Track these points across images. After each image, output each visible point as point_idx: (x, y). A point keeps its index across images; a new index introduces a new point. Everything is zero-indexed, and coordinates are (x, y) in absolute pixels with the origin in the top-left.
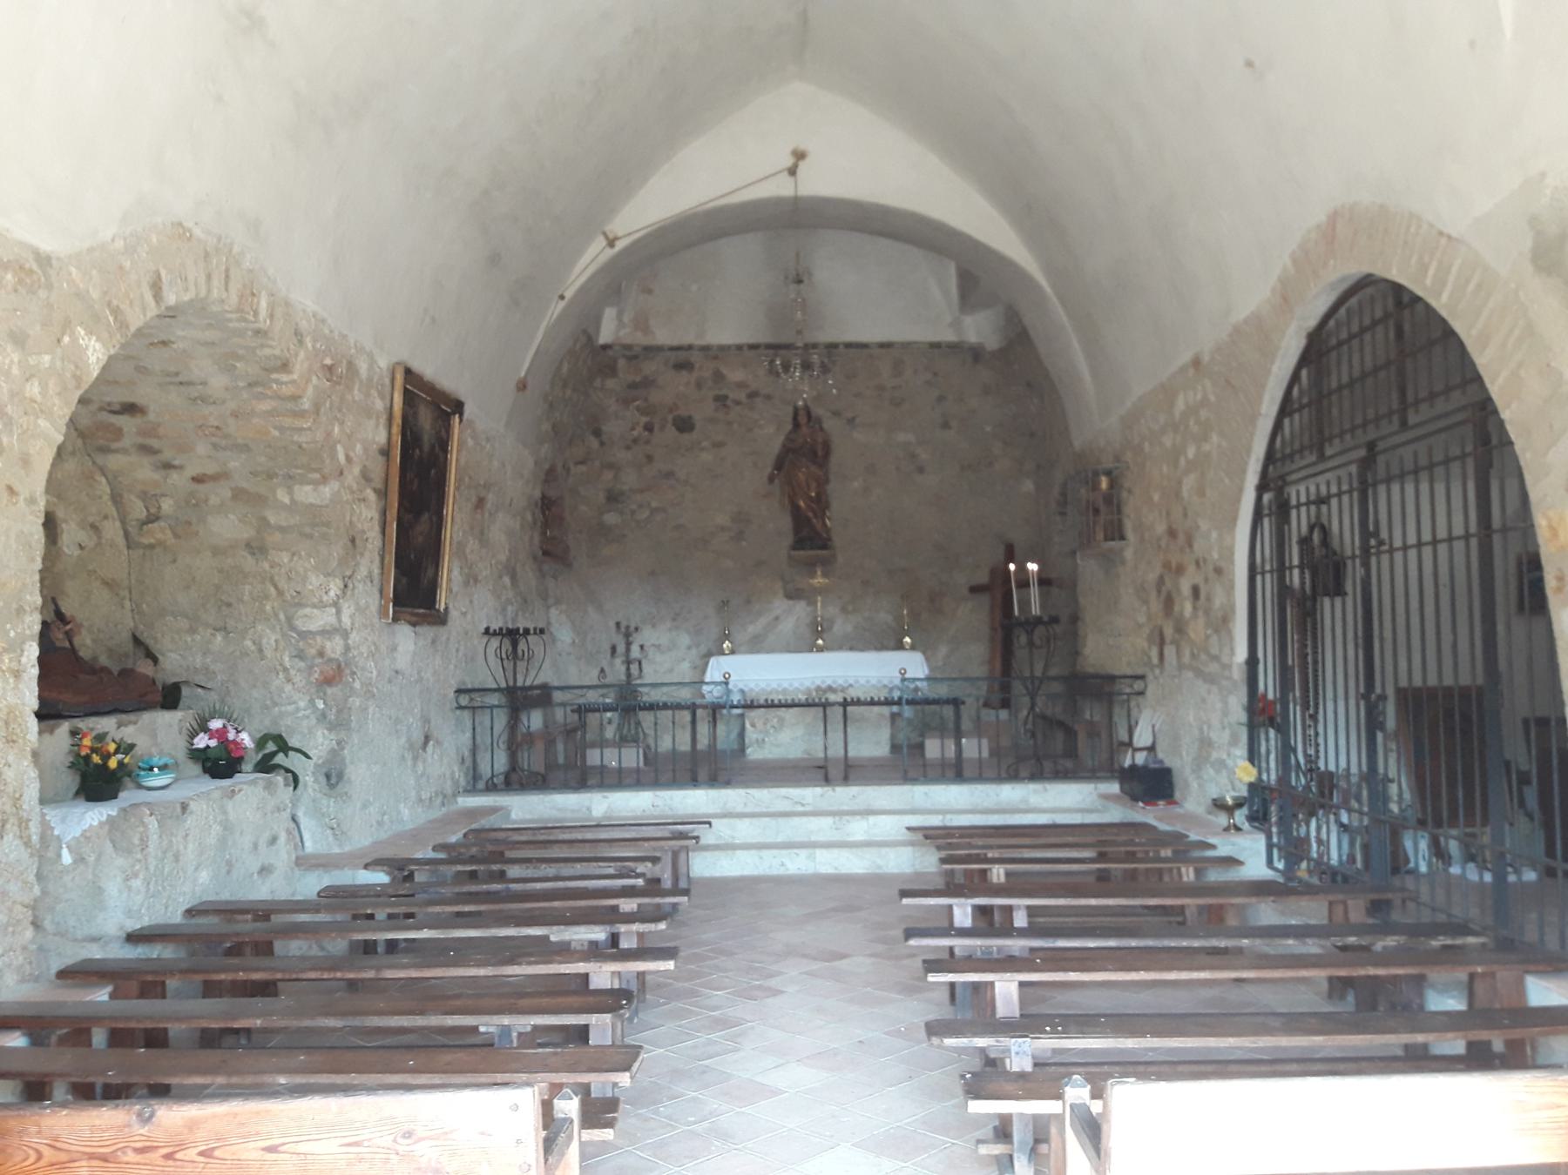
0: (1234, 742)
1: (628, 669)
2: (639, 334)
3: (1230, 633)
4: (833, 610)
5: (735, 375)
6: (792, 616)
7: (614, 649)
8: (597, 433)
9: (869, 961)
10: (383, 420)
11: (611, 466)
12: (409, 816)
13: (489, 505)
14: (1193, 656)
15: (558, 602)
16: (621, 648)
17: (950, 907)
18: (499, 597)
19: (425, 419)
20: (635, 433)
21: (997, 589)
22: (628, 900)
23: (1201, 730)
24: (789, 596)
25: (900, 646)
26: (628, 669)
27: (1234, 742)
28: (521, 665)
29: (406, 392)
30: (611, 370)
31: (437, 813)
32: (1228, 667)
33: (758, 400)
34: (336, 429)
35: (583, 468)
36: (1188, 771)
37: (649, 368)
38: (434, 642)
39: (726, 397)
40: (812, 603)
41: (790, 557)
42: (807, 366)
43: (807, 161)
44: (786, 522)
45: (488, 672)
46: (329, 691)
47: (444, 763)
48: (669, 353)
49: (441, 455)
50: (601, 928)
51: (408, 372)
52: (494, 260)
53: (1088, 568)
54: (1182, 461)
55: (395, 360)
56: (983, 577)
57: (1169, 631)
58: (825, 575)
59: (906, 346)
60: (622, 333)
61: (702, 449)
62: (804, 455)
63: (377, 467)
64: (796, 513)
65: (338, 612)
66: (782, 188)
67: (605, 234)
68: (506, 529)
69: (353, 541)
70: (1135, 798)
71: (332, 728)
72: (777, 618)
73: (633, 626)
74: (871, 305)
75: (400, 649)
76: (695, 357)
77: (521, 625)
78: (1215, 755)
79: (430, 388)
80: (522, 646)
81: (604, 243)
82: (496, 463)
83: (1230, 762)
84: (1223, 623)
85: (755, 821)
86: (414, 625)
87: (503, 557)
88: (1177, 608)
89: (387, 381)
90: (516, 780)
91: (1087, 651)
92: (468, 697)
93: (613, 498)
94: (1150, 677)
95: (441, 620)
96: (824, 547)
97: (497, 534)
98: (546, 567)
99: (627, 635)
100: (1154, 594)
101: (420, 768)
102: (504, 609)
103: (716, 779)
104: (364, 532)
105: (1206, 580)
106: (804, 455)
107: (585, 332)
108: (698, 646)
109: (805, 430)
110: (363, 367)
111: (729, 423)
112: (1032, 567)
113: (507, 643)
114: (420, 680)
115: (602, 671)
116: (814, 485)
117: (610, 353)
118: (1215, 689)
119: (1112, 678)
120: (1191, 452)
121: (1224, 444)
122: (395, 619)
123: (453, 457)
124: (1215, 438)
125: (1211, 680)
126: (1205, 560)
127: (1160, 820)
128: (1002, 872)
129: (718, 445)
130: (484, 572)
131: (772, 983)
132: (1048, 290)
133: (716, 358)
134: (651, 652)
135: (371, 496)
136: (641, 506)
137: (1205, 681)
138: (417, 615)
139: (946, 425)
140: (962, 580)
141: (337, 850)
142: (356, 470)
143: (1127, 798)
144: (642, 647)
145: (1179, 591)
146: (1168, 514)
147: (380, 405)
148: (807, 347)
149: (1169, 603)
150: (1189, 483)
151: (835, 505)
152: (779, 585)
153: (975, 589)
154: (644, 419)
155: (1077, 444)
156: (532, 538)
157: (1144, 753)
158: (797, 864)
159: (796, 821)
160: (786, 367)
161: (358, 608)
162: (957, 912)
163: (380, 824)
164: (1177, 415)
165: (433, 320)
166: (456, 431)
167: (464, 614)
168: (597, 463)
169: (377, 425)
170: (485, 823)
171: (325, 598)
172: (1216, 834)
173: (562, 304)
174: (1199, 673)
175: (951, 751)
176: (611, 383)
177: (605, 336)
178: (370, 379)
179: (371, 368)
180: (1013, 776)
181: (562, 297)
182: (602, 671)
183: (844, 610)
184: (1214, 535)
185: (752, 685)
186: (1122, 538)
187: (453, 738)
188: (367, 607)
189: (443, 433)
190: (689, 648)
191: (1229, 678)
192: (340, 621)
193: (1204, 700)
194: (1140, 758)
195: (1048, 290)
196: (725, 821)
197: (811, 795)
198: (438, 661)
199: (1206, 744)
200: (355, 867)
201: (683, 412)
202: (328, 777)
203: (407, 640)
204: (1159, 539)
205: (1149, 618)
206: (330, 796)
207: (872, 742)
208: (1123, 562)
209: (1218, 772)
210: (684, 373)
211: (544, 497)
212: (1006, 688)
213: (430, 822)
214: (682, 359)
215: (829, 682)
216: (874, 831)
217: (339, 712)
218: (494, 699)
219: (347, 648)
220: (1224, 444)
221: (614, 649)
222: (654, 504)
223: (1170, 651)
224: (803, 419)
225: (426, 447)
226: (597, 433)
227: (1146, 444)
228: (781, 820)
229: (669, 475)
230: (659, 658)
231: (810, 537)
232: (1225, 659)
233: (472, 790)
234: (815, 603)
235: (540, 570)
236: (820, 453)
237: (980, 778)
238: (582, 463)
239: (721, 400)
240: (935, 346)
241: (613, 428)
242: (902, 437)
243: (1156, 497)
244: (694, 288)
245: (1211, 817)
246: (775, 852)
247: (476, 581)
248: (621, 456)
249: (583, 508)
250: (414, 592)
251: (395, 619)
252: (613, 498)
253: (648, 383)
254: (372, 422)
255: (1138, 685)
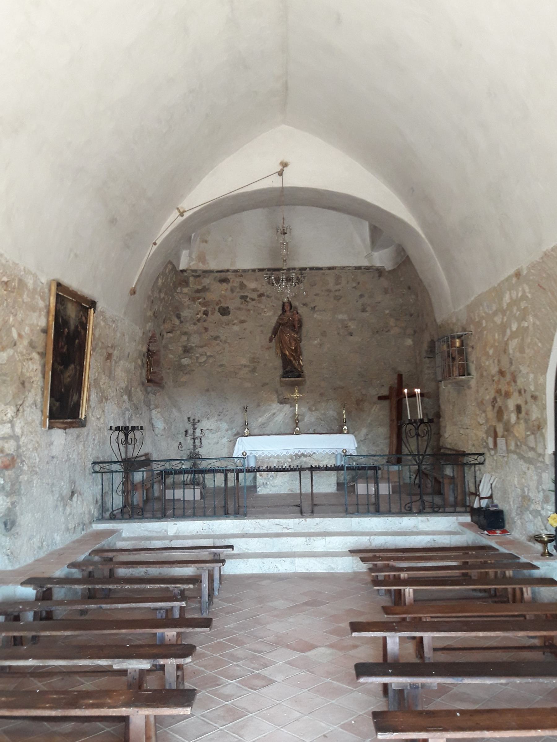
0: (546, 500)
1: (194, 443)
2: (200, 264)
3: (543, 436)
4: (304, 410)
5: (252, 285)
6: (281, 414)
7: (186, 432)
8: (178, 317)
9: (328, 651)
10: (43, 313)
11: (185, 333)
12: (60, 540)
13: (115, 358)
14: (517, 445)
15: (156, 407)
16: (190, 431)
17: (385, 639)
18: (121, 407)
19: (72, 312)
20: (199, 316)
21: (395, 399)
22: (170, 629)
23: (523, 490)
24: (281, 403)
25: (341, 432)
26: (194, 443)
27: (546, 500)
28: (130, 447)
29: (58, 296)
30: (185, 282)
31: (76, 537)
32: (542, 455)
33: (263, 298)
34: (11, 319)
35: (171, 335)
36: (514, 514)
37: (206, 281)
38: (78, 436)
39: (247, 297)
40: (293, 406)
41: (281, 381)
42: (289, 280)
43: (289, 167)
44: (278, 362)
45: (112, 450)
46: (7, 473)
47: (84, 506)
48: (216, 274)
49: (82, 332)
50: (148, 661)
51: (59, 285)
52: (113, 221)
53: (446, 389)
54: (508, 332)
55: (52, 278)
56: (385, 392)
57: (500, 430)
58: (299, 392)
59: (343, 268)
60: (192, 263)
61: (234, 324)
62: (288, 327)
63: (40, 340)
64: (284, 356)
65: (13, 427)
66: (275, 183)
67: (178, 209)
68: (125, 370)
69: (23, 383)
70: (482, 527)
71: (8, 495)
72: (274, 414)
73: (197, 419)
74: (324, 246)
75: (55, 443)
76: (230, 275)
77: (130, 425)
78: (533, 507)
79: (73, 294)
80: (131, 435)
81: (178, 214)
82: (119, 334)
83: (543, 513)
84: (538, 428)
85: (260, 540)
86: (65, 429)
87: (123, 385)
88: (505, 417)
89: (46, 290)
90: (130, 512)
91: (446, 435)
92: (100, 466)
93: (187, 350)
94: (487, 455)
95: (82, 424)
96: (299, 376)
97: (119, 373)
98: (149, 389)
99: (194, 424)
100: (489, 408)
101: (68, 509)
102: (124, 414)
103: (239, 512)
104: (31, 377)
105: (526, 403)
106: (288, 327)
107: (170, 263)
108: (232, 429)
109: (288, 313)
110: (30, 282)
111: (249, 310)
112: (417, 391)
113: (122, 436)
114: (69, 459)
115: (180, 444)
116: (293, 343)
117: (185, 274)
118: (532, 467)
119: (464, 454)
120: (514, 327)
121: (538, 323)
122: (51, 427)
123: (90, 332)
124: (531, 319)
125: (529, 461)
126: (525, 391)
127: (501, 544)
128: (411, 591)
129: (243, 322)
130: (112, 393)
131: (265, 672)
132: (423, 236)
133: (241, 276)
134: (207, 433)
135: (35, 356)
136: (201, 355)
137: (525, 462)
138: (67, 423)
139: (364, 310)
140: (374, 392)
141: (10, 568)
142: (25, 342)
143: (476, 526)
144: (201, 430)
145: (506, 407)
146: (499, 361)
147: (41, 304)
148: (289, 269)
149: (500, 414)
150: (513, 344)
151: (305, 353)
152: (275, 397)
153: (381, 398)
154: (204, 309)
155: (439, 321)
156: (141, 373)
157: (486, 500)
158: (284, 567)
159: (284, 539)
160: (278, 280)
161: (27, 423)
162: (389, 641)
163: (40, 548)
164: (505, 306)
165: (76, 256)
166: (92, 318)
167: (98, 419)
168: (178, 332)
169: (40, 316)
170: (104, 543)
171: (5, 418)
172: (537, 559)
173: (155, 247)
174: (522, 457)
175: (372, 490)
176: (185, 290)
177: (182, 266)
178: (35, 290)
179: (35, 283)
180: (408, 511)
181: (155, 244)
182: (180, 444)
183: (310, 409)
184: (531, 376)
185: (260, 453)
186: (469, 374)
187: (91, 488)
188: (33, 421)
189: (84, 318)
190: (227, 431)
191: (543, 462)
192: (13, 431)
193: (525, 473)
194: (484, 503)
195: (423, 236)
196: (243, 539)
197: (292, 523)
198: (81, 447)
199: (525, 499)
200: (16, 583)
201: (223, 305)
202: (5, 524)
203: (60, 437)
204: (493, 376)
205: (487, 420)
206: (6, 536)
207: (326, 484)
208: (469, 387)
209: (535, 517)
210: (224, 284)
211: (149, 350)
212: (399, 450)
213: (74, 542)
214: (223, 277)
215: (302, 451)
216: (328, 547)
217: (13, 485)
218: (115, 467)
219: (19, 447)
220: (538, 323)
221: (186, 432)
222: (208, 354)
223: (501, 442)
224: (287, 307)
225: (72, 327)
226: (178, 317)
227: (484, 322)
228: (276, 539)
229: (216, 338)
230: (211, 436)
231: (292, 371)
232: (540, 451)
233: (101, 519)
234: (295, 406)
235: (146, 391)
236: (297, 326)
237: (389, 513)
238: (169, 332)
239: (244, 298)
240: (359, 268)
241: (185, 313)
242: (340, 317)
243: (491, 352)
244: (230, 239)
245: (531, 544)
246: (272, 559)
247: (107, 399)
248: (191, 328)
249: (171, 356)
250: (64, 408)
251: (51, 427)
252: (187, 350)
253: (205, 289)
254: (36, 314)
255: (480, 459)
